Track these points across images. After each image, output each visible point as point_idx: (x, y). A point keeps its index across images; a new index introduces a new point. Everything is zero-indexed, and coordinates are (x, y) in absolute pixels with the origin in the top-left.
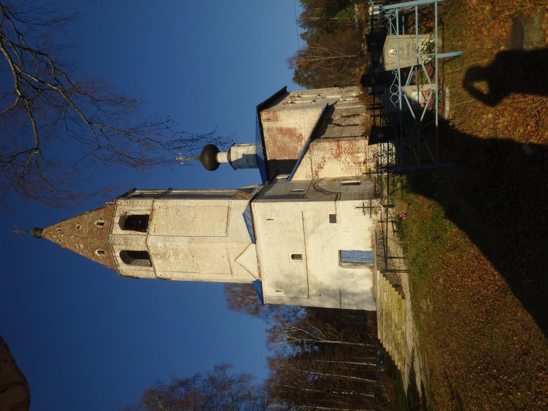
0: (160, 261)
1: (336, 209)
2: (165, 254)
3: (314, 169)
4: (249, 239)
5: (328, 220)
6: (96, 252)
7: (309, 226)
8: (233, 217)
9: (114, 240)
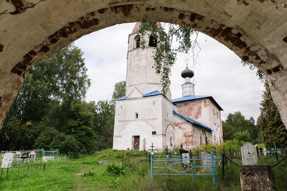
3: (179, 124)
4: (145, 93)
7: (150, 122)
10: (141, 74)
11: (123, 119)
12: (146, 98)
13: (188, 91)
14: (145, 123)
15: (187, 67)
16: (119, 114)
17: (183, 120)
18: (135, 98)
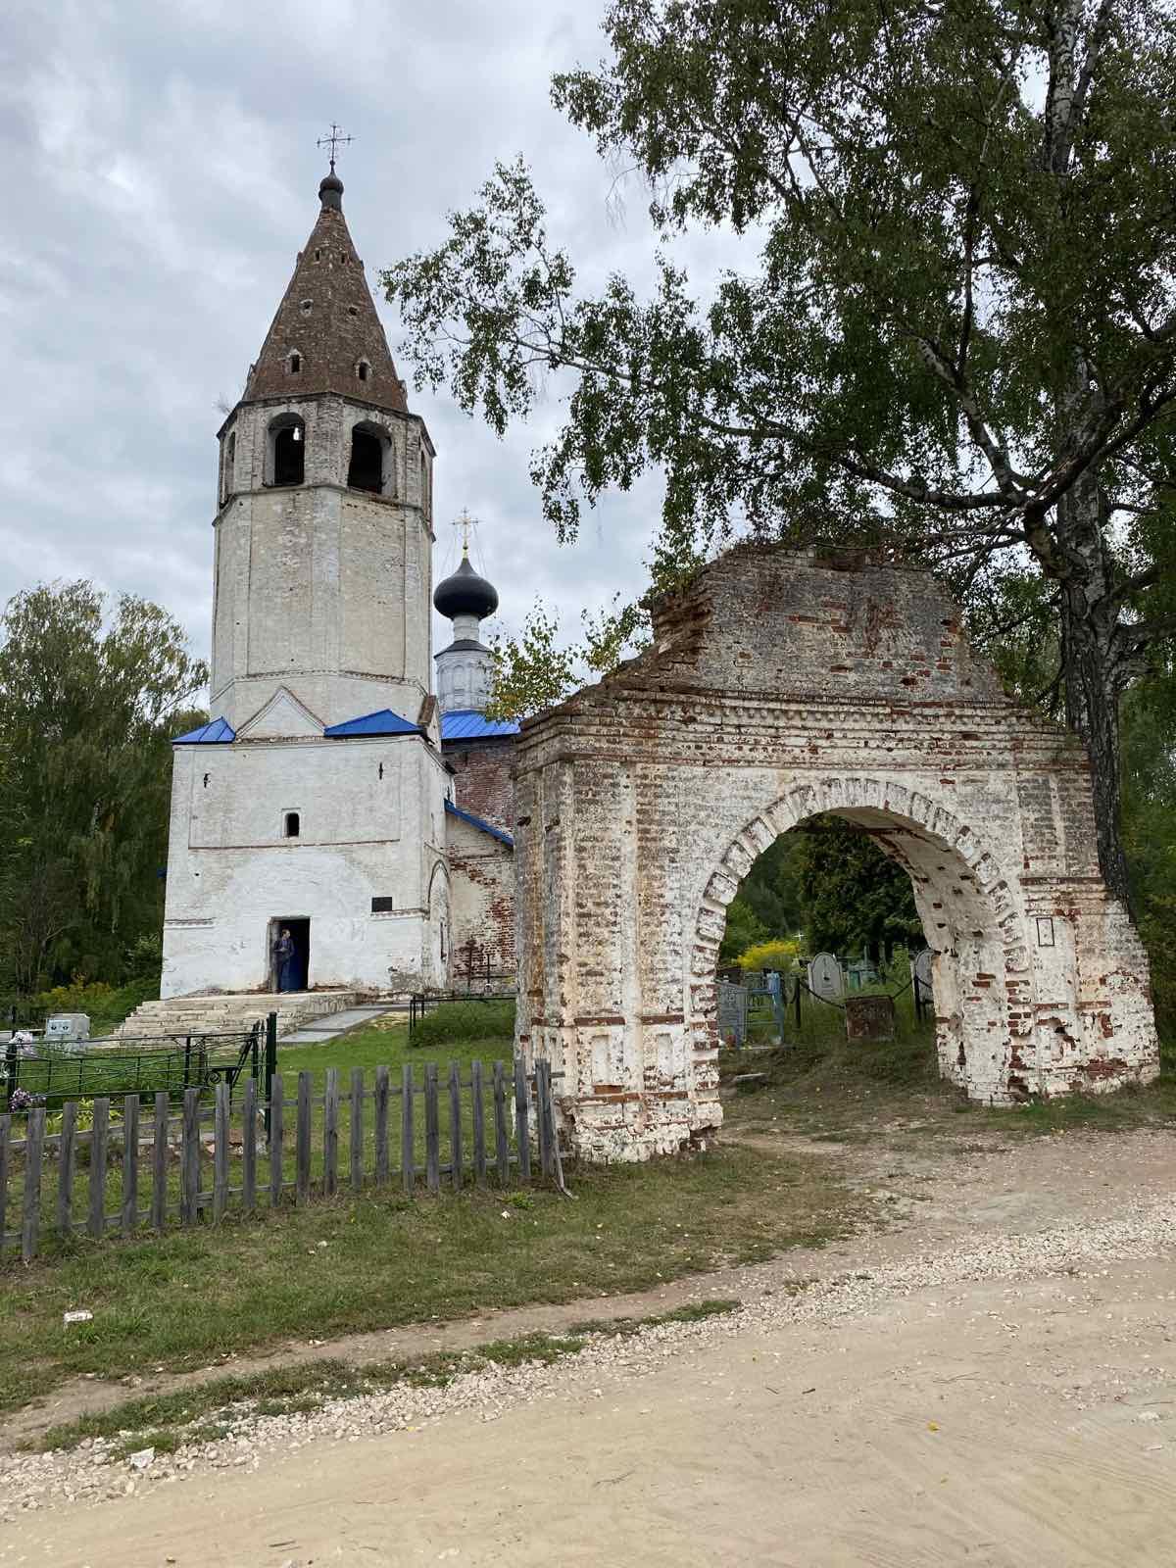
0: (278, 508)
1: (403, 912)
2: (297, 523)
3: (470, 862)
4: (334, 722)
5: (378, 895)
6: (295, 352)
7: (364, 855)
8: (382, 687)
9: (330, 407)
10: (310, 624)
11: (215, 839)
12: (340, 742)
13: (467, 688)
14: (340, 860)
15: (465, 562)
16: (195, 813)
17: (491, 842)
18: (284, 741)
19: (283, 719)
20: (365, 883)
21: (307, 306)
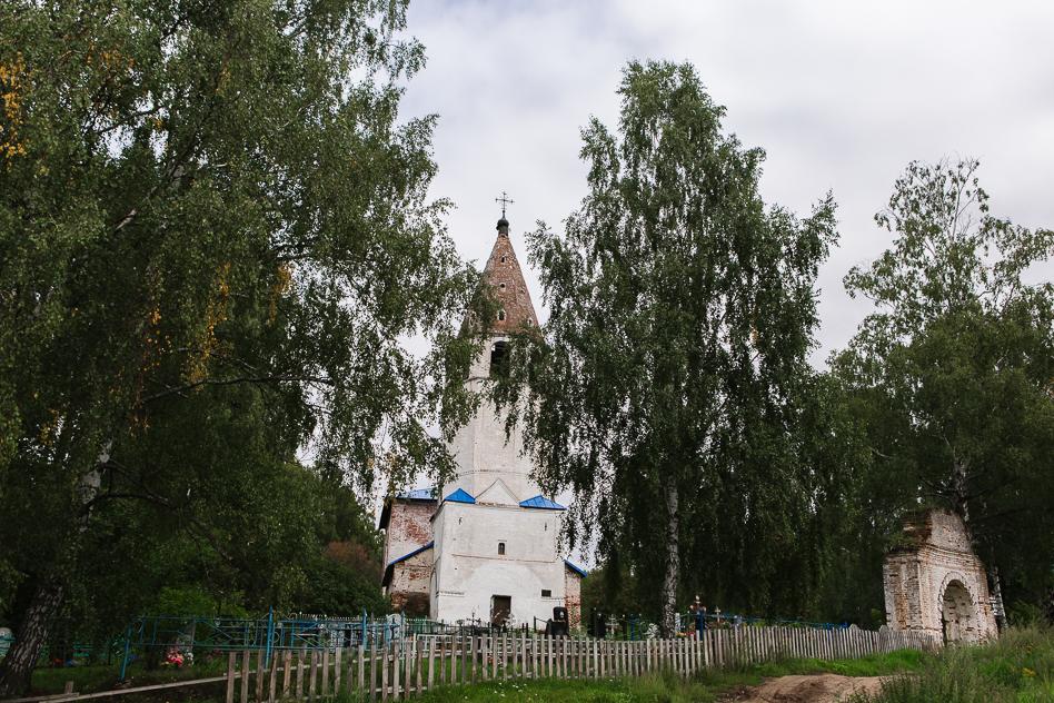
7: (539, 568)
11: (463, 552)
14: (526, 569)
18: (500, 506)
19: (497, 494)
20: (539, 582)
21: (503, 286)
